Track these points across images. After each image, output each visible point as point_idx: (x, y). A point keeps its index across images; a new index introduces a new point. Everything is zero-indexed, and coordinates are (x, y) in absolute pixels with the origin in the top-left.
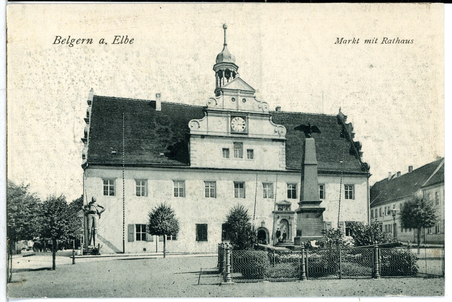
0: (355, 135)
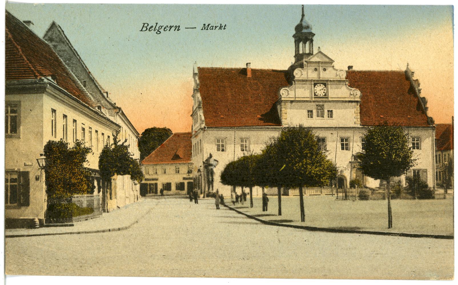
0: (422, 91)
